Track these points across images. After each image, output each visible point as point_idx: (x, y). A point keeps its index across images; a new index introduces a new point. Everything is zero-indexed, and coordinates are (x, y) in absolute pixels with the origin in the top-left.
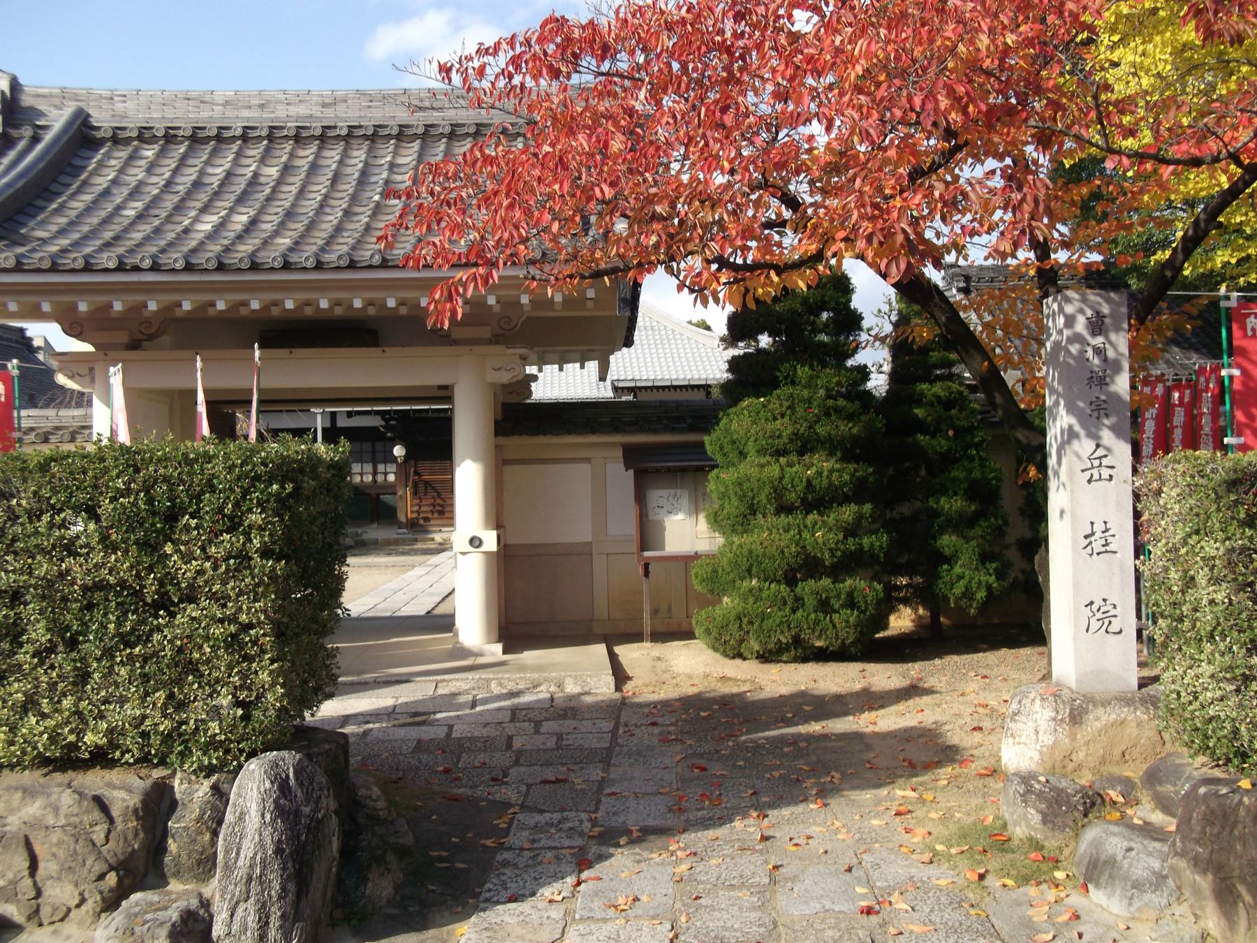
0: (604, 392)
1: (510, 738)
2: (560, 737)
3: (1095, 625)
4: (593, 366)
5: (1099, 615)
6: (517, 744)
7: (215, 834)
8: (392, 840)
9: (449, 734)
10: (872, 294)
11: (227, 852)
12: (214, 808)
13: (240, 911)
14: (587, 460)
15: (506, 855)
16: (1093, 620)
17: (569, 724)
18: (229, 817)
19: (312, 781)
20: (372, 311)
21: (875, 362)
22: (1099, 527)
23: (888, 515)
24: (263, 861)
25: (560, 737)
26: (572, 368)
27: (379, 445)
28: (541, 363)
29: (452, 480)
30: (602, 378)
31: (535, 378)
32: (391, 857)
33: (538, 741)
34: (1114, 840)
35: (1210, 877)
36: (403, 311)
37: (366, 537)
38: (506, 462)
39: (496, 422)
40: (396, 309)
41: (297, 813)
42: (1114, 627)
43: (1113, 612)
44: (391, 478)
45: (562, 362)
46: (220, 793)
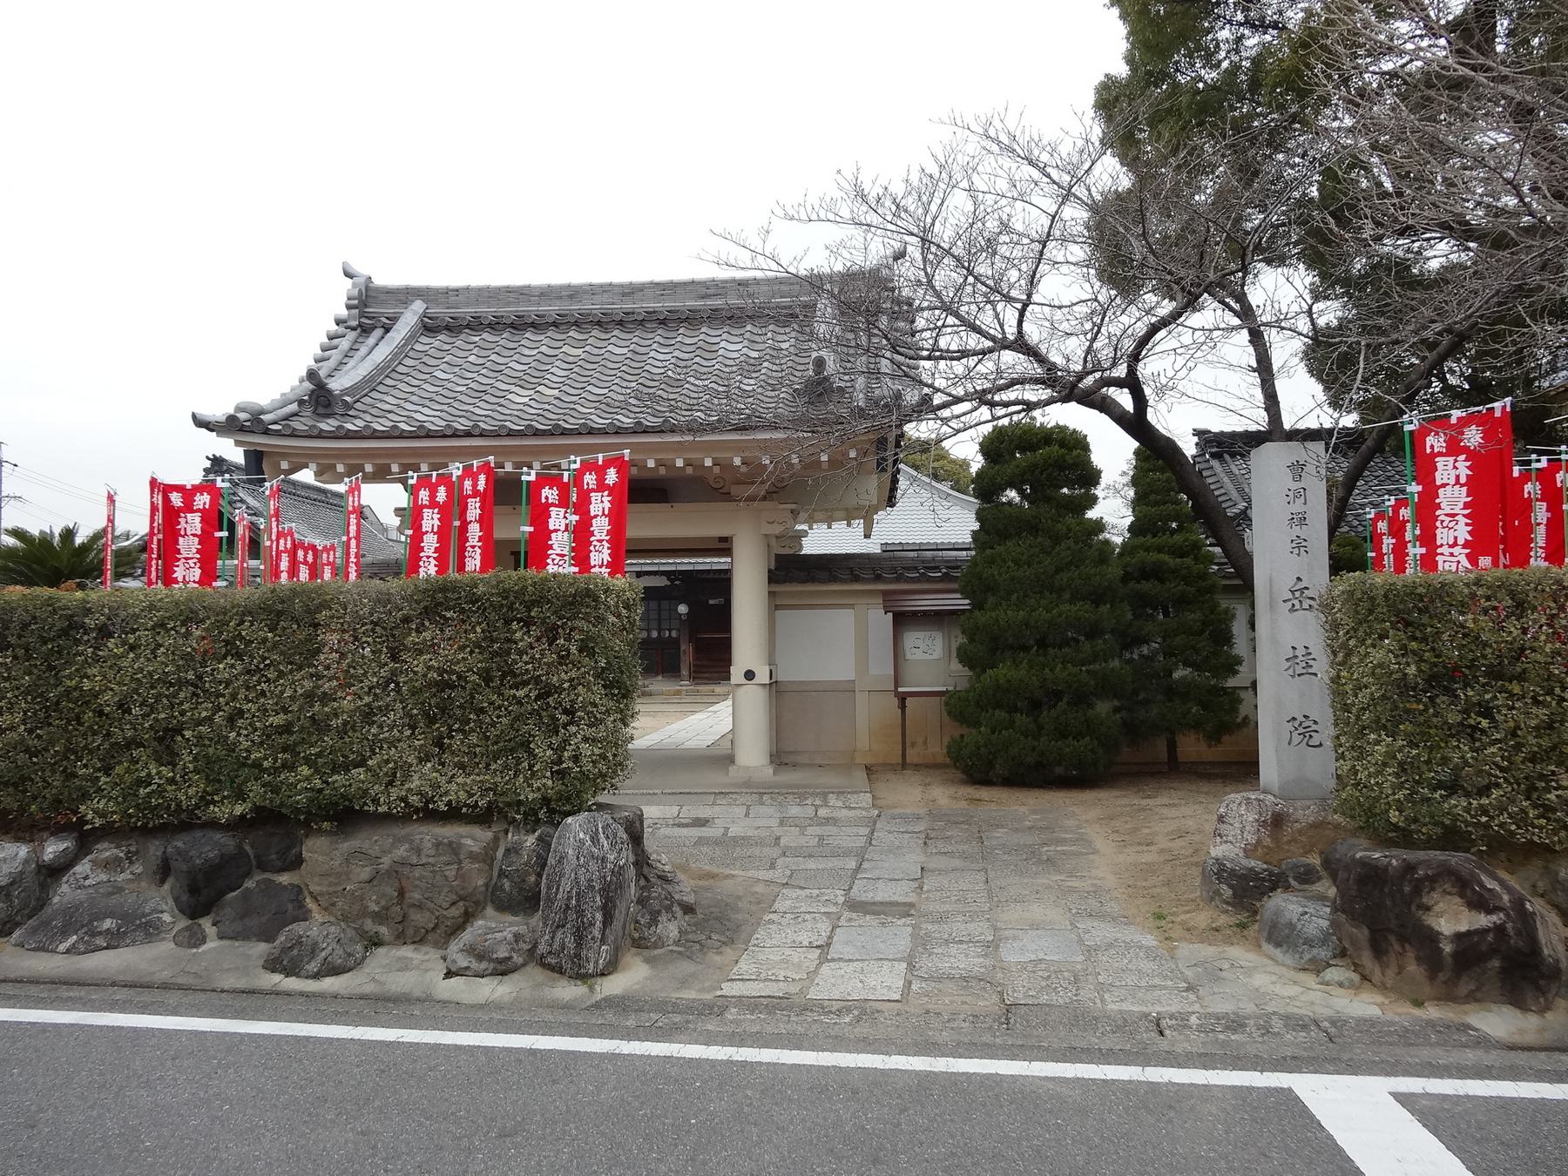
0: (872, 547)
1: (778, 838)
2: (821, 838)
3: (1296, 739)
4: (859, 524)
5: (1301, 730)
6: (783, 842)
7: (540, 875)
8: (677, 897)
9: (725, 834)
10: (1112, 452)
11: (549, 888)
12: (539, 856)
13: (559, 935)
14: (851, 606)
15: (772, 916)
16: (1295, 734)
17: (833, 830)
18: (551, 861)
19: (615, 835)
20: (662, 471)
21: (1113, 510)
22: (1300, 652)
23: (1128, 656)
24: (578, 894)
25: (821, 838)
26: (840, 526)
27: (665, 604)
28: (811, 521)
29: (729, 639)
30: (867, 536)
31: (805, 534)
32: (676, 908)
33: (803, 841)
34: (1291, 907)
35: (1366, 931)
36: (689, 470)
37: (651, 688)
38: (777, 607)
39: (770, 571)
40: (683, 469)
41: (604, 859)
42: (1314, 742)
43: (1314, 727)
44: (674, 634)
45: (829, 522)
46: (545, 842)
